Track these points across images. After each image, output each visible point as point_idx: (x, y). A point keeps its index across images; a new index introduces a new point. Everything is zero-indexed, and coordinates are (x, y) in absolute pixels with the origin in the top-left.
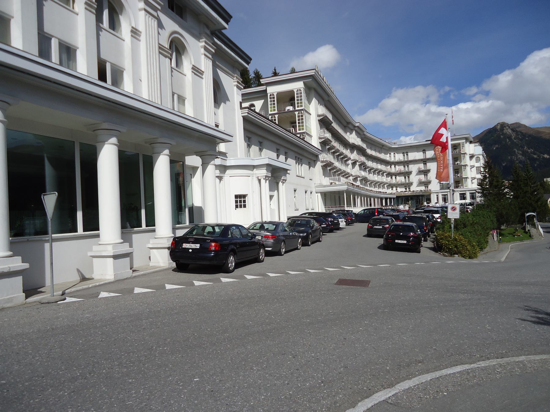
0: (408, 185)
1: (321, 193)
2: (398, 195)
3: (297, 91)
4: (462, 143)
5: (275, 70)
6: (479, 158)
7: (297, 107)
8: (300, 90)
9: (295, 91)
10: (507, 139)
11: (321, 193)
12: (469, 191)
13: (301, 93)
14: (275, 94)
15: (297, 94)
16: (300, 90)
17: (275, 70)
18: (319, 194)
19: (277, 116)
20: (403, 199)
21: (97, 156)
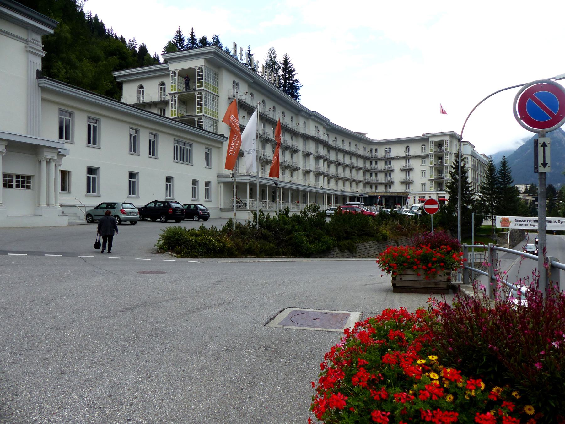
0: (389, 184)
1: (224, 184)
2: (370, 194)
3: (199, 69)
4: (446, 141)
5: (249, 51)
6: (468, 158)
7: (198, 87)
8: (201, 68)
9: (197, 69)
10: (557, 144)
11: (224, 184)
12: (419, 194)
13: (202, 72)
14: (177, 72)
15: (198, 72)
16: (201, 68)
17: (249, 51)
18: (222, 185)
19: (177, 96)
20: (370, 200)
21: (512, 155)
